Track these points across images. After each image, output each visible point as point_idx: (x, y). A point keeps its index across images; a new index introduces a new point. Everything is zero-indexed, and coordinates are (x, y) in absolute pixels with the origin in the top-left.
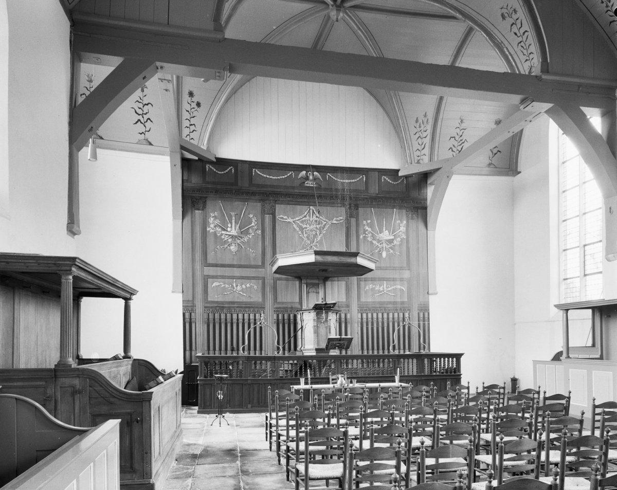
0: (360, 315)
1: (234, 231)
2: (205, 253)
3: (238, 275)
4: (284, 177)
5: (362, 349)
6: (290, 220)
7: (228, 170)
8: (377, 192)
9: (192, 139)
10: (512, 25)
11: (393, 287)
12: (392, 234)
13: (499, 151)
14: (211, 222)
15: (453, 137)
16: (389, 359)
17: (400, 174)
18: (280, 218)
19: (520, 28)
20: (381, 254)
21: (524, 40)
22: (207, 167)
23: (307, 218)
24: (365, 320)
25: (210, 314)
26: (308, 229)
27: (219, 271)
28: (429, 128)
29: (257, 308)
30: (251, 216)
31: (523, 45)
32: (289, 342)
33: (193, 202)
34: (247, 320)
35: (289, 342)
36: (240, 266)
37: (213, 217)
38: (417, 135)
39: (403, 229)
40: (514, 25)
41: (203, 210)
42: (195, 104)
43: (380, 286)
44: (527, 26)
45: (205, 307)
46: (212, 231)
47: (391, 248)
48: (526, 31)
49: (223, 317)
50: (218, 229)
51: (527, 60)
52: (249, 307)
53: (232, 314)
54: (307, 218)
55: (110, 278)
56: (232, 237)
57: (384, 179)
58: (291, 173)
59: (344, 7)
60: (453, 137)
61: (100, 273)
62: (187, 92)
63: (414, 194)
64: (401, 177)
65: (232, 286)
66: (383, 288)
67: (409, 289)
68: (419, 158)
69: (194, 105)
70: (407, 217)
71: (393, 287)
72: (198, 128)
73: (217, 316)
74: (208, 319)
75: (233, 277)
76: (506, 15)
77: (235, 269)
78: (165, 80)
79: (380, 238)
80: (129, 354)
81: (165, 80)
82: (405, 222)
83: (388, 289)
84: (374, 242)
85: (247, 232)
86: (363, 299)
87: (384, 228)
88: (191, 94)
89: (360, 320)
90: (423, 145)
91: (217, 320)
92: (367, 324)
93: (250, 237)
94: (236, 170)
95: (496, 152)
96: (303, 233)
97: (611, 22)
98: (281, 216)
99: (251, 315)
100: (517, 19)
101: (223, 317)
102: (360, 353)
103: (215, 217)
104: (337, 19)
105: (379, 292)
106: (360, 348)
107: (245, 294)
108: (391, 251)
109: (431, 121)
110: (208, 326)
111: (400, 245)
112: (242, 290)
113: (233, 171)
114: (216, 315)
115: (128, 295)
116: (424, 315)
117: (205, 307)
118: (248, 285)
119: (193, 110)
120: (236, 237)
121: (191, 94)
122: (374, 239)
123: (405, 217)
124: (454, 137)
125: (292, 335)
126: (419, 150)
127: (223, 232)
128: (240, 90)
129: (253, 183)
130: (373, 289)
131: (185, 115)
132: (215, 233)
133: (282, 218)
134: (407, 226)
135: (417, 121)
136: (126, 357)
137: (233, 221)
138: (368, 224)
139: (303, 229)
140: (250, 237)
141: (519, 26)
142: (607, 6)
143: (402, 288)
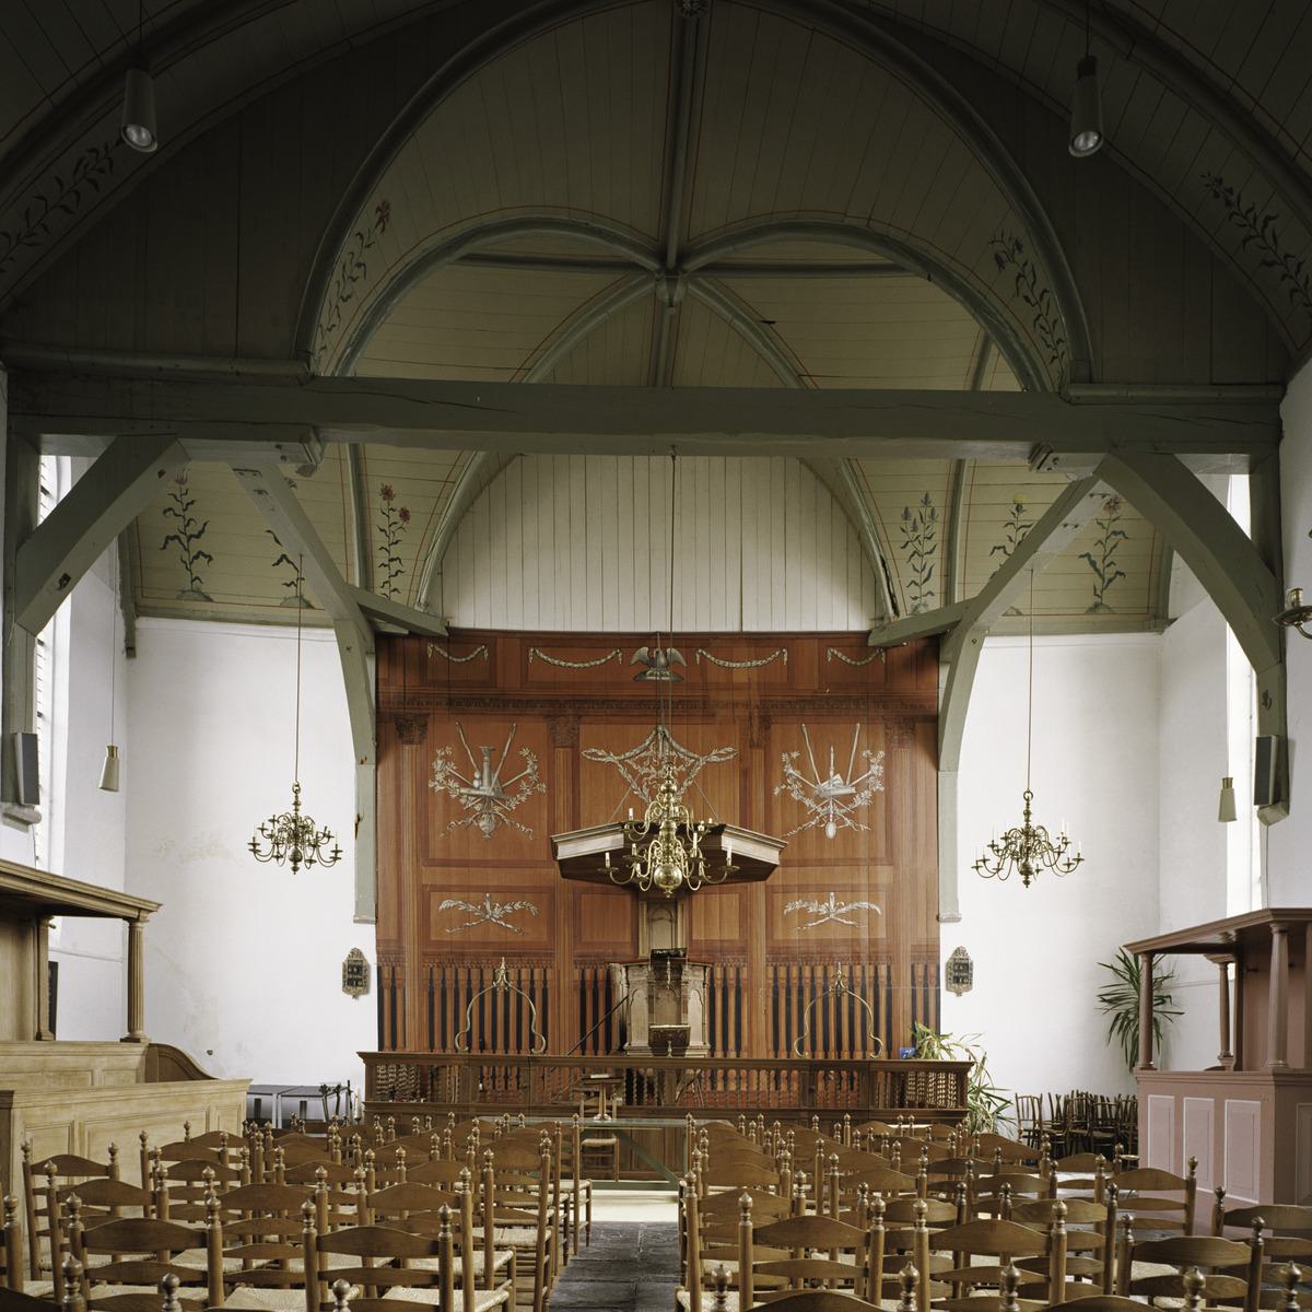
0: (771, 969)
1: (484, 786)
2: (423, 839)
3: (495, 883)
4: (598, 663)
5: (776, 1048)
6: (612, 758)
7: (476, 653)
8: (816, 687)
9: (395, 590)
10: (1017, 280)
11: (850, 907)
12: (851, 782)
13: (1121, 574)
14: (438, 768)
15: (999, 548)
16: (790, 1071)
17: (871, 642)
18: (590, 755)
19: (1033, 284)
20: (823, 831)
21: (1044, 312)
22: (430, 649)
23: (649, 753)
24: (782, 982)
25: (435, 970)
26: (653, 776)
27: (455, 876)
28: (938, 529)
29: (536, 955)
30: (525, 752)
31: (1044, 324)
32: (595, 1033)
33: (399, 727)
34: (465, 982)
35: (595, 1033)
36: (498, 865)
37: (441, 758)
38: (910, 549)
39: (877, 769)
40: (1022, 279)
41: (420, 743)
42: (397, 514)
43: (821, 902)
44: (1044, 280)
45: (425, 954)
46: (439, 788)
47: (848, 815)
48: (1045, 291)
49: (462, 976)
50: (453, 784)
51: (1054, 358)
52: (520, 955)
53: (482, 971)
54: (649, 753)
55: (27, 871)
56: (484, 799)
57: (833, 653)
58: (614, 653)
59: (684, 272)
60: (999, 548)
61: (12, 867)
62: (379, 488)
63: (908, 685)
64: (874, 648)
65: (484, 908)
66: (828, 909)
67: (892, 912)
68: (917, 602)
69: (395, 516)
70: (888, 741)
71: (850, 907)
72: (408, 566)
73: (449, 973)
74: (431, 980)
75: (484, 889)
76: (1004, 257)
77: (490, 870)
78: (246, 470)
79: (820, 792)
80: (139, 1033)
81: (246, 470)
82: (882, 754)
83: (839, 911)
84: (808, 802)
85: (515, 790)
86: (779, 935)
87: (832, 768)
88: (387, 493)
89: (771, 982)
90: (927, 571)
91: (450, 983)
92: (789, 992)
93: (523, 799)
94: (493, 655)
95: (1112, 576)
96: (640, 785)
97: (1245, 241)
98: (594, 750)
99: (523, 971)
100: (1025, 264)
101: (462, 976)
102: (772, 1056)
103: (446, 759)
104: (671, 299)
105: (818, 916)
106: (771, 1046)
107: (509, 926)
108: (849, 822)
109: (941, 514)
110: (431, 995)
111: (871, 808)
112: (505, 917)
113: (486, 655)
114: (448, 971)
115: (134, 914)
116: (926, 968)
117: (425, 954)
118: (517, 906)
119: (393, 528)
120: (491, 798)
121: (387, 493)
122: (806, 796)
123: (882, 739)
124: (1004, 547)
125: (602, 1016)
126: (917, 584)
127: (463, 791)
128: (501, 476)
129: (530, 679)
130: (803, 912)
131: (378, 539)
132: (446, 793)
133: (595, 755)
134: (888, 763)
135: (906, 516)
136: (132, 1039)
137: (486, 765)
138: (792, 761)
139: (642, 777)
140: (523, 799)
141: (1030, 279)
142: (1228, 203)
143: (874, 907)
